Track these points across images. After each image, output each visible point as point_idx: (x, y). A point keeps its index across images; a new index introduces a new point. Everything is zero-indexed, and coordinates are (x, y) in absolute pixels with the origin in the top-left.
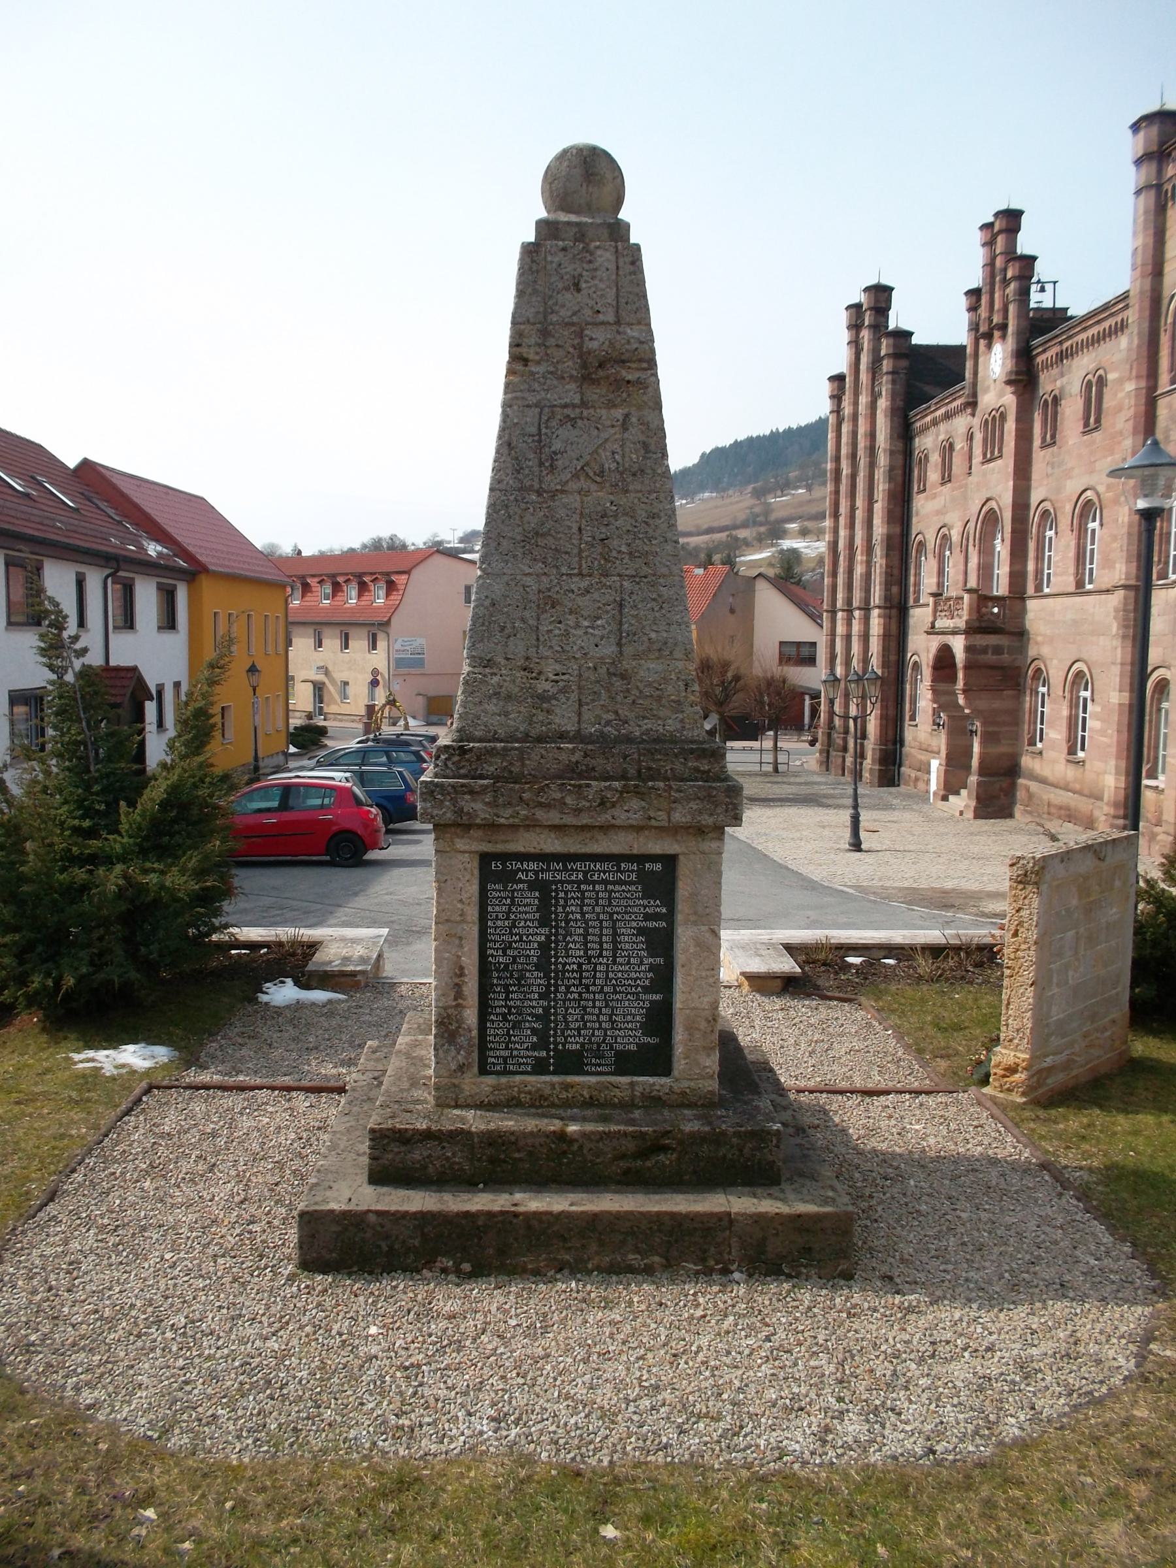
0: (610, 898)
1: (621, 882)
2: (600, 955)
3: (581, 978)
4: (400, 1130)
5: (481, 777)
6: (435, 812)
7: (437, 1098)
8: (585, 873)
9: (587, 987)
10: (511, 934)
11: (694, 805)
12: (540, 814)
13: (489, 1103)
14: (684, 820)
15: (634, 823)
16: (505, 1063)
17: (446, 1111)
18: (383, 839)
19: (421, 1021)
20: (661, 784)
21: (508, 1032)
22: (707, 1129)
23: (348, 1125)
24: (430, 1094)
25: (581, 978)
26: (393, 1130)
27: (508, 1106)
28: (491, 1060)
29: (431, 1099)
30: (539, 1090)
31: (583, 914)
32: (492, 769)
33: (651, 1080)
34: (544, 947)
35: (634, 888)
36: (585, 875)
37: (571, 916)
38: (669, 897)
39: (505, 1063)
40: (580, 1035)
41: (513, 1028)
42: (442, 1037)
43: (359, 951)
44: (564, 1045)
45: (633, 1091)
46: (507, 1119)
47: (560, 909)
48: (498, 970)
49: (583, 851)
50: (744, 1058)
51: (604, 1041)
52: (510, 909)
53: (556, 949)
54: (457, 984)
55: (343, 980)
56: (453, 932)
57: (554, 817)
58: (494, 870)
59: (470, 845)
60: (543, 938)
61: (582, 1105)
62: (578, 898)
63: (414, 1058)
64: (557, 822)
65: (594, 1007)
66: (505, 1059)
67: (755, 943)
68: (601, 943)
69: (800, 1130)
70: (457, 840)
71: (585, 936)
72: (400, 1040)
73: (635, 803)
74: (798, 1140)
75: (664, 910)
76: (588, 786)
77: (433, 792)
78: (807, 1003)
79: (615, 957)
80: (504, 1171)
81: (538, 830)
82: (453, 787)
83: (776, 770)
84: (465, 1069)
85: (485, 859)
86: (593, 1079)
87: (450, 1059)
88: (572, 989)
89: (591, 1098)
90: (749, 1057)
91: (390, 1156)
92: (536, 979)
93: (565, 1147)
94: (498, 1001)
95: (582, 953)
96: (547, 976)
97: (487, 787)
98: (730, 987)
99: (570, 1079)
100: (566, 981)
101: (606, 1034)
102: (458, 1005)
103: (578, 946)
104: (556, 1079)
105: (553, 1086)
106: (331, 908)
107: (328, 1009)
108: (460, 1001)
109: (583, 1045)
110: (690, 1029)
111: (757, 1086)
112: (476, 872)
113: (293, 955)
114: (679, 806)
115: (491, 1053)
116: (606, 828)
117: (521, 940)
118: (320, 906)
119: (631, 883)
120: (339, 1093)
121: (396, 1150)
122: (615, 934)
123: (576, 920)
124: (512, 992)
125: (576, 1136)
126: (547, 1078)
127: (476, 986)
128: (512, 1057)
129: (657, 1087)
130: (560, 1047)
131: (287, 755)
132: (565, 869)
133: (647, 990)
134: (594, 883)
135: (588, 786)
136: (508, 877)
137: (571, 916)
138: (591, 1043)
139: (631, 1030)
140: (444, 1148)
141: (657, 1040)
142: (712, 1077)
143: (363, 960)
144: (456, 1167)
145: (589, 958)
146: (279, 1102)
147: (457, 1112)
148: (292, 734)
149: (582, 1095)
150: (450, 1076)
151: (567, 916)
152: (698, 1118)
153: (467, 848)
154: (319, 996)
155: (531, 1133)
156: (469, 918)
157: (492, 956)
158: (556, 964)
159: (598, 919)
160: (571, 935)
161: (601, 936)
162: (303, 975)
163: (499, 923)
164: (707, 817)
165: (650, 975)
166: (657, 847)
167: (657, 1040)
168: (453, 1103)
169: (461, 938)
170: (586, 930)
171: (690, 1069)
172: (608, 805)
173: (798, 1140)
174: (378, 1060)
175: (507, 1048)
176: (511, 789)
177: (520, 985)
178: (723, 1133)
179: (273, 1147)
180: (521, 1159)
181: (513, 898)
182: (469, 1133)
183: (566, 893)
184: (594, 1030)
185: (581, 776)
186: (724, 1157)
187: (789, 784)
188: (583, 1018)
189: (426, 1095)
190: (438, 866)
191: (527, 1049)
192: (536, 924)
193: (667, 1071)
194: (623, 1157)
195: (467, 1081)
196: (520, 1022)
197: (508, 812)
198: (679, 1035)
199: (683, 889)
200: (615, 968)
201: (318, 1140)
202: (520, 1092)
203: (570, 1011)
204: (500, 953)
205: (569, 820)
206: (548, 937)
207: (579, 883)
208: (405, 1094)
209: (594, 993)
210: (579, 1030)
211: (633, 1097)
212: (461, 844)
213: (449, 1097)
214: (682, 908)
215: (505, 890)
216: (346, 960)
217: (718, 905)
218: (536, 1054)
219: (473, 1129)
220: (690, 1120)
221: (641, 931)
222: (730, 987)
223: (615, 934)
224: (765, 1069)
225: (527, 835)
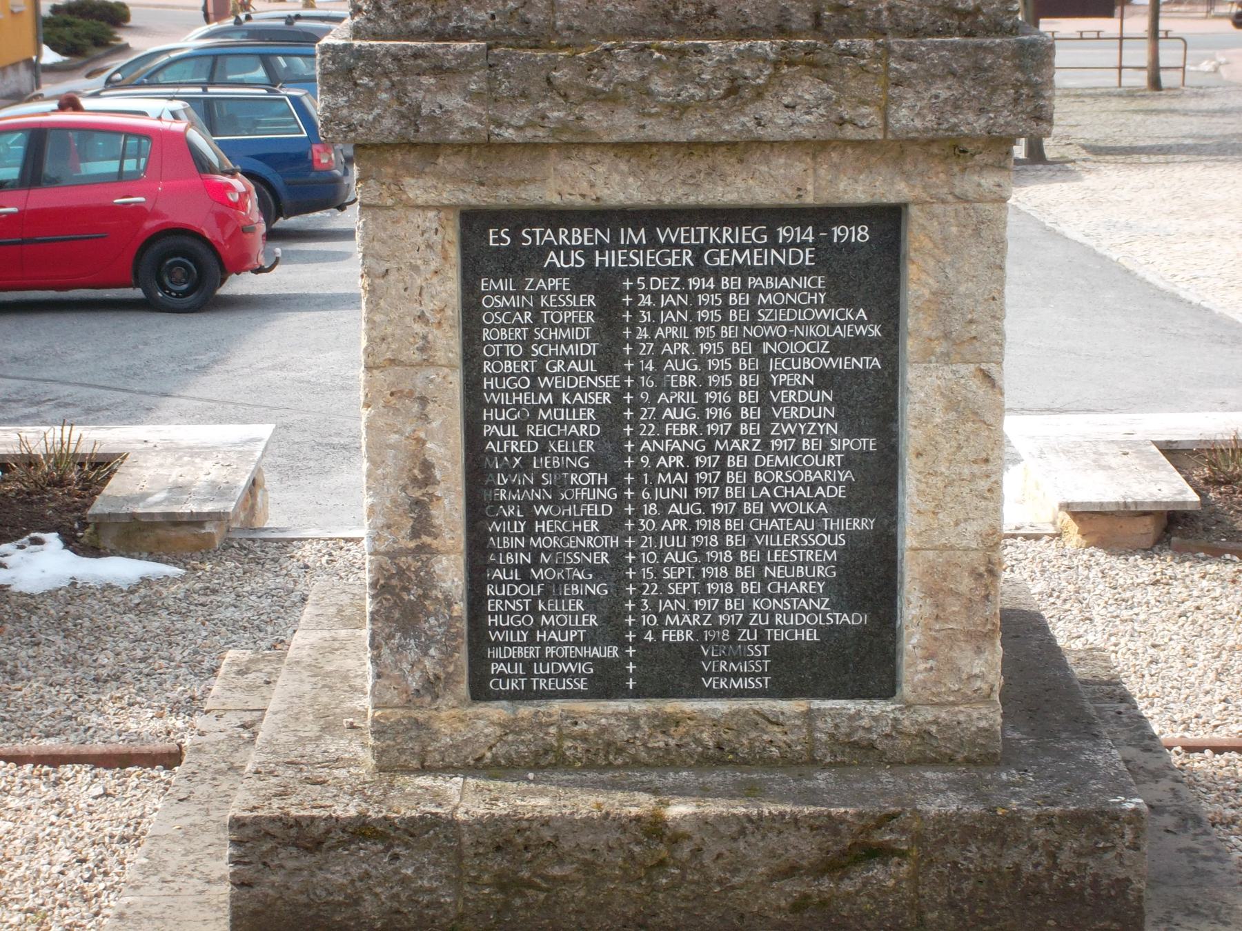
0: (753, 308)
1: (777, 271)
2: (735, 433)
3: (691, 486)
4: (298, 822)
5: (459, 35)
6: (357, 116)
7: (380, 754)
8: (698, 252)
9: (706, 503)
10: (535, 389)
11: (942, 91)
12: (594, 118)
13: (495, 762)
14: (918, 123)
15: (807, 133)
16: (529, 673)
17: (400, 780)
18: (260, 251)
19: (345, 599)
20: (868, 44)
21: (534, 607)
22: (977, 809)
23: (186, 821)
24: (364, 745)
25: (691, 486)
26: (287, 823)
27: (537, 767)
28: (495, 668)
29: (368, 759)
30: (604, 730)
31: (694, 343)
32: (483, 16)
33: (851, 706)
34: (609, 417)
35: (806, 282)
36: (697, 258)
37: (667, 348)
38: (888, 308)
39: (529, 673)
40: (691, 611)
41: (545, 596)
42: (388, 619)
43: (206, 472)
44: (657, 633)
45: (811, 732)
46: (533, 793)
47: (643, 333)
48: (507, 471)
49: (691, 200)
50: (1063, 666)
51: (745, 623)
52: (531, 335)
53: (635, 422)
54: (417, 502)
55: (173, 533)
56: (406, 386)
57: (625, 124)
58: (493, 247)
59: (435, 193)
60: (606, 398)
61: (699, 763)
62: (682, 307)
63: (328, 674)
64: (631, 134)
65: (722, 548)
66: (528, 664)
67: (1096, 442)
68: (735, 408)
69: (1190, 820)
70: (408, 181)
71: (700, 391)
72: (298, 640)
73: (808, 89)
74: (1185, 841)
75: (876, 332)
76: (701, 50)
77: (350, 70)
78: (1212, 568)
79: (766, 438)
80: (528, 906)
81: (589, 154)
82: (396, 58)
83: (1155, 83)
84: (439, 688)
85: (473, 222)
86: (722, 706)
87: (406, 666)
88: (674, 509)
89: (719, 747)
90: (1076, 671)
91: (277, 879)
92: (592, 489)
93: (662, 851)
94: (509, 538)
95: (693, 429)
96: (616, 481)
97: (471, 56)
98: (1037, 538)
99: (672, 706)
100: (658, 493)
101: (749, 607)
102: (421, 548)
103: (684, 413)
104: (640, 706)
105: (634, 720)
106: (146, 400)
107: (143, 600)
108: (426, 539)
109: (698, 632)
110: (933, 592)
111: (1091, 722)
112: (454, 253)
113: (61, 483)
114: (910, 94)
115: (497, 653)
116: (744, 148)
117: (557, 403)
118: (125, 396)
119: (800, 271)
120: (168, 767)
121: (291, 864)
122: (766, 386)
123: (679, 357)
124: (541, 518)
125: (686, 828)
126: (622, 706)
127: (461, 504)
128: (543, 660)
129: (865, 722)
130: (649, 637)
131: (38, 70)
132: (653, 242)
133: (839, 508)
134: (717, 273)
135: (701, 50)
136: (521, 263)
137: (667, 348)
138: (716, 627)
139: (806, 596)
140: (396, 857)
141: (864, 619)
142: (987, 699)
143: (218, 491)
144: (425, 899)
145: (710, 441)
146: (33, 787)
147: (425, 781)
148: (46, 22)
149: (698, 742)
150: (407, 705)
151: (658, 348)
152: (954, 786)
153: (432, 197)
154: (120, 569)
155: (588, 822)
156: (440, 356)
157: (494, 438)
158: (636, 454)
159: (728, 353)
160: (668, 390)
161: (734, 391)
162: (84, 525)
163: (508, 366)
164: (971, 117)
165: (845, 476)
166: (856, 188)
167: (864, 619)
168: (415, 764)
169: (423, 401)
170: (702, 378)
171: (938, 682)
172: (747, 93)
173: (1185, 841)
174: (251, 688)
175: (531, 641)
176: (527, 60)
177: (556, 502)
178: (1014, 819)
179: (23, 879)
180: (565, 880)
181: (537, 311)
182: (452, 823)
183: (656, 296)
184: (722, 598)
185: (683, 28)
186: (1017, 870)
187: (1185, 113)
188: (697, 573)
189: (355, 747)
190: (369, 239)
191: (576, 642)
192: (590, 366)
193: (888, 690)
194: (791, 871)
195: (443, 715)
196: (558, 583)
197: (522, 113)
198: (912, 607)
199: (918, 282)
200: (767, 461)
201: (121, 862)
202: (561, 737)
203: (669, 556)
204: (512, 431)
205: (660, 130)
206: (617, 395)
207: (684, 273)
208: (309, 748)
209: (722, 517)
210: (689, 597)
211: (812, 744)
212: (416, 190)
213: (405, 749)
214: (917, 324)
215: (519, 291)
216: (179, 489)
217: (997, 317)
218: (596, 652)
219: (460, 816)
220: (937, 792)
221: (824, 379)
222: (1037, 538)
223: (766, 386)
224: (1111, 696)
225: (565, 167)
